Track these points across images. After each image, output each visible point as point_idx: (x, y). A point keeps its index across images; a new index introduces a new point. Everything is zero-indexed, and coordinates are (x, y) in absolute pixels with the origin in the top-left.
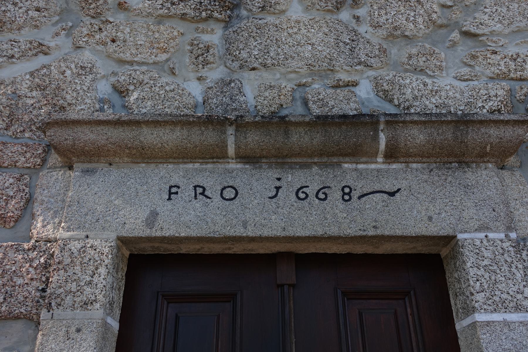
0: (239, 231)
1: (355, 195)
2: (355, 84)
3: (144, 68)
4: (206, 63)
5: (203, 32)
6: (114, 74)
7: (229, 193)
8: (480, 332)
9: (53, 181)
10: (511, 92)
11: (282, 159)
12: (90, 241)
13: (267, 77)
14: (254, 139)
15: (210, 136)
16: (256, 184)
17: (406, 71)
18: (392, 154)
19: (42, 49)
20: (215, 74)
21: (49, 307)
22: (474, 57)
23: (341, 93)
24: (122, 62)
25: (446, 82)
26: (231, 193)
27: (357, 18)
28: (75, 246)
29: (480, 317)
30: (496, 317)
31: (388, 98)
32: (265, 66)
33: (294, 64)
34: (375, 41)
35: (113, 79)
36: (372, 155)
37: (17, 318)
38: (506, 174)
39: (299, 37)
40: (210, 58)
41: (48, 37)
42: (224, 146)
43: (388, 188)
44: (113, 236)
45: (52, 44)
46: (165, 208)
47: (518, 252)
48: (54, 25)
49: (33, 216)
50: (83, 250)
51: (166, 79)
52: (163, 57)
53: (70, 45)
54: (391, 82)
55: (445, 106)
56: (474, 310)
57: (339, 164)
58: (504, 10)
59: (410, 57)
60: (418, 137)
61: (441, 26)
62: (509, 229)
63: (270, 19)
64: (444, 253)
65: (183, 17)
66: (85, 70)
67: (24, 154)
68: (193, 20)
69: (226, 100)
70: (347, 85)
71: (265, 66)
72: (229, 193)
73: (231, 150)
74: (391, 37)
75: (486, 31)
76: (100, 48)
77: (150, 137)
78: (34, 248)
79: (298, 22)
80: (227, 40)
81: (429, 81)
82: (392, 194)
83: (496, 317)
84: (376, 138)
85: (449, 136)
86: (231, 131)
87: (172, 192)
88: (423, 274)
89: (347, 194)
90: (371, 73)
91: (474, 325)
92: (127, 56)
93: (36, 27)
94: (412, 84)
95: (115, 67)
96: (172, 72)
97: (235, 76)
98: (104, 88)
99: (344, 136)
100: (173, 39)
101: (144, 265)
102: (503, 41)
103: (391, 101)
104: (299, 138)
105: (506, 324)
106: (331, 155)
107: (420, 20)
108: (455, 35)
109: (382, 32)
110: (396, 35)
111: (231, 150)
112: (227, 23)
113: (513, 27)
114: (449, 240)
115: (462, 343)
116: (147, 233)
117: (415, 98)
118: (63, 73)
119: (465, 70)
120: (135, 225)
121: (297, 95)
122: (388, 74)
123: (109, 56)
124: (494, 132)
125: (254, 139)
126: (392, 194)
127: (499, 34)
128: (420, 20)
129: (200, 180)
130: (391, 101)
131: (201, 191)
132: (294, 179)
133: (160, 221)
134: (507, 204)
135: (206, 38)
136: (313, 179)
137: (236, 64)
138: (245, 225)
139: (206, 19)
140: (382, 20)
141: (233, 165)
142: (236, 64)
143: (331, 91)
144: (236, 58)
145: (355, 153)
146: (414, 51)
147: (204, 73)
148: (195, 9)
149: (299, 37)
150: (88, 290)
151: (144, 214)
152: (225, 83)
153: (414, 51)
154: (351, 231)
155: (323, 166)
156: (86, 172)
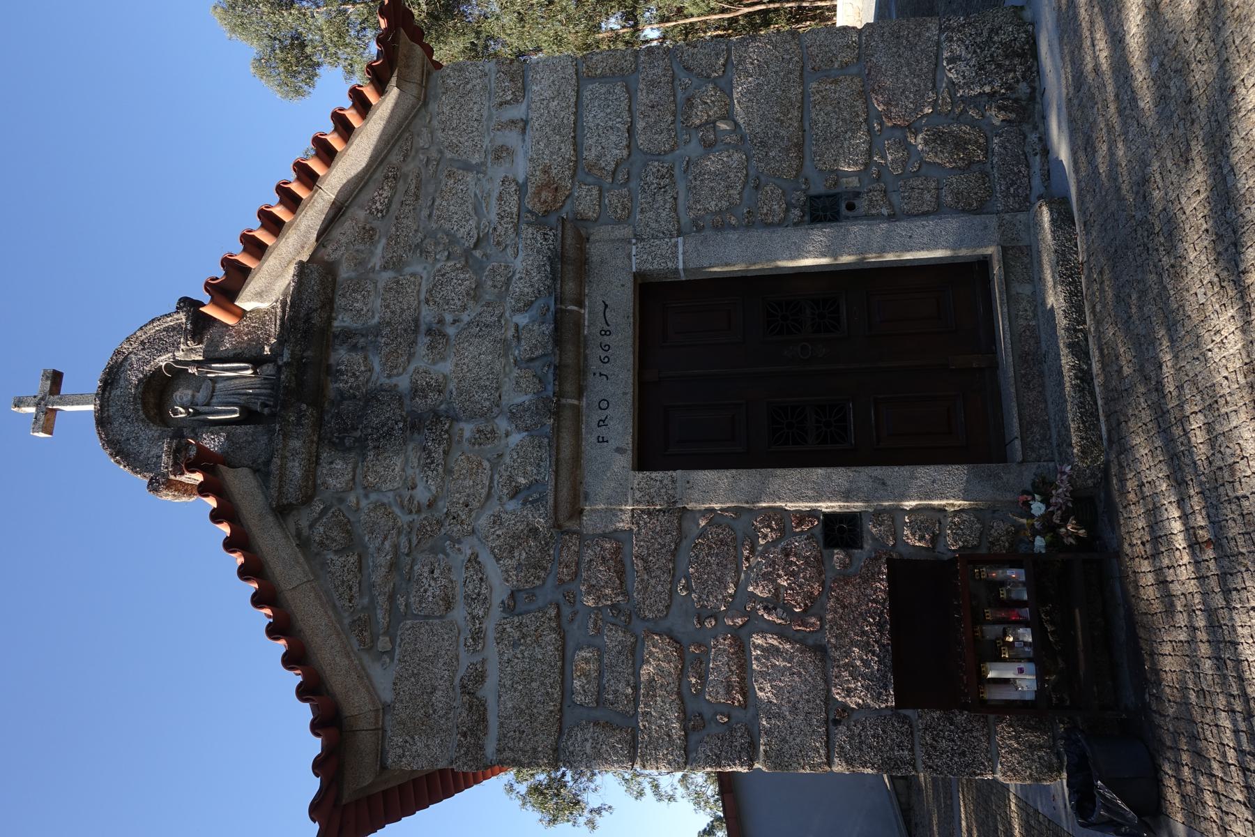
0: (629, 397)
1: (606, 328)
2: (517, 326)
3: (496, 477)
4: (493, 431)
5: (461, 437)
6: (500, 498)
7: (604, 405)
8: (691, 265)
9: (590, 523)
10: (529, 224)
11: (581, 372)
12: (635, 486)
13: (507, 386)
14: (569, 387)
15: (567, 414)
16: (598, 388)
17: (507, 289)
18: (580, 304)
19: (474, 560)
20: (503, 424)
21: (675, 502)
22: (499, 243)
23: (525, 334)
24: (489, 496)
25: (519, 264)
26: (603, 405)
27: (455, 321)
28: (638, 495)
29: (681, 266)
30: (681, 257)
31: (529, 305)
32: (497, 389)
33: (497, 367)
34: (479, 309)
35: (505, 499)
36: (581, 316)
37: (680, 524)
38: (592, 238)
39: (472, 364)
40: (489, 429)
41: (461, 557)
42: (573, 406)
43: (602, 308)
44: (632, 473)
45: (469, 552)
46: (613, 444)
47: (643, 240)
48: (447, 555)
49: (616, 531)
50: (640, 490)
51: (507, 460)
52: (486, 464)
53: (470, 538)
54: (518, 301)
55: (539, 267)
56: (677, 269)
57: (585, 337)
58: (456, 216)
59: (495, 287)
60: (570, 287)
61: (467, 262)
62: (630, 242)
63: (452, 386)
64: (639, 281)
65: (446, 453)
66: (497, 520)
67: (569, 548)
68: (450, 445)
69: (528, 414)
70: (517, 330)
71: (497, 389)
72: (604, 405)
73: (576, 402)
74: (476, 298)
75: (474, 233)
76: (474, 514)
77: (566, 452)
78: (638, 524)
79: (457, 365)
80: (471, 418)
81: (518, 276)
82: (606, 306)
83: (681, 257)
84: (571, 312)
85: (570, 267)
86: (563, 401)
87: (602, 440)
88: (653, 293)
89: (607, 333)
90: (507, 314)
91: (684, 270)
92: (484, 492)
93: (449, 570)
94: (518, 287)
95: (495, 500)
96: (500, 456)
97: (506, 409)
98: (512, 505)
99: (565, 330)
100: (468, 458)
101: (647, 457)
102: (484, 221)
103: (532, 302)
104: (569, 359)
105: (684, 253)
106: (581, 342)
107: (462, 276)
108: (478, 253)
109: (471, 304)
110: (475, 294)
111: (576, 402)
112: (455, 419)
113: (472, 213)
114: (636, 275)
115: (692, 278)
116: (630, 452)
117: (532, 286)
118: (499, 536)
119: (510, 251)
120: (623, 462)
121: (524, 365)
122: (510, 302)
123: (482, 507)
124: (569, 241)
125: (569, 387)
126: (606, 306)
127: (479, 224)
128: (462, 276)
129: (594, 424)
130: (532, 302)
131: (602, 423)
132: (594, 365)
133: (624, 446)
134: (613, 241)
135: (467, 434)
136: (595, 354)
137: (496, 410)
138: (625, 394)
139: (450, 437)
140: (459, 303)
141: (584, 403)
142: (496, 410)
143: (523, 343)
144: (490, 409)
145: (578, 325)
146: (490, 283)
147: (502, 432)
148: (439, 444)
149: (472, 364)
150: (665, 482)
151: (618, 456)
152: (512, 416)
153: (490, 283)
154: (629, 331)
155: (586, 347)
156: (586, 498)
